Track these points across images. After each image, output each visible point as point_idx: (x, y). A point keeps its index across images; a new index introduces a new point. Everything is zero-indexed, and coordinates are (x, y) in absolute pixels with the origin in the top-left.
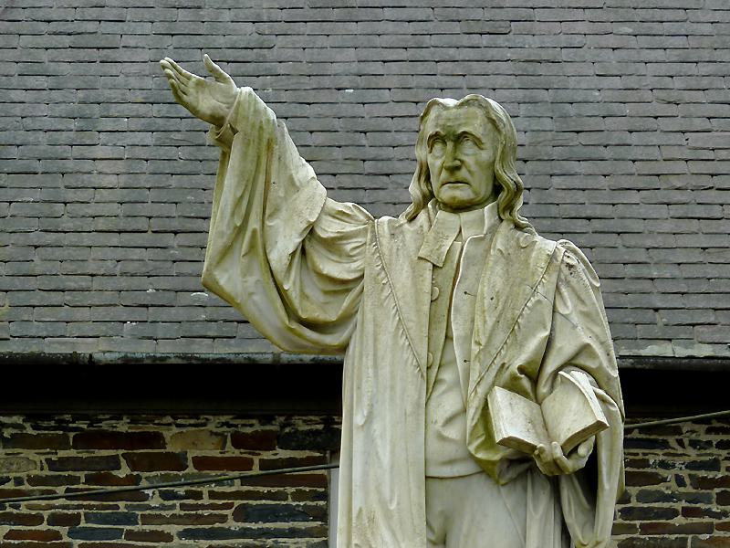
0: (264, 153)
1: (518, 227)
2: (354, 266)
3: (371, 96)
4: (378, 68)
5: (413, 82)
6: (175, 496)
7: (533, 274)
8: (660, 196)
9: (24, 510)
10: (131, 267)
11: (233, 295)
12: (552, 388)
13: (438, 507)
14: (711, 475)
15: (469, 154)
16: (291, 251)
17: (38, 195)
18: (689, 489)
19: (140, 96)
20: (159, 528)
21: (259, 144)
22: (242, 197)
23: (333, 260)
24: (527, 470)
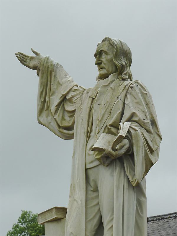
21: (47, 73)
23: (71, 105)
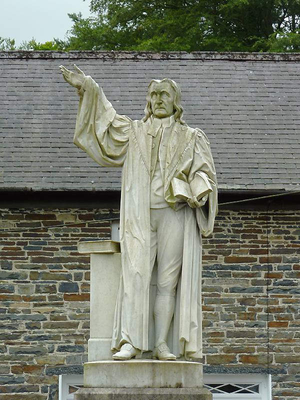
0: (95, 98)
1: (182, 124)
2: (126, 137)
3: (125, 103)
4: (128, 94)
5: (139, 98)
6: (60, 236)
7: (187, 139)
8: (223, 136)
9: (9, 241)
10: (45, 159)
11: (84, 146)
12: (193, 178)
13: (154, 219)
14: (239, 229)
15: (165, 99)
16: (104, 131)
17: (13, 135)
18: (232, 234)
19: (47, 103)
20: (54, 246)
21: (93, 95)
22: (87, 113)
24: (185, 206)
